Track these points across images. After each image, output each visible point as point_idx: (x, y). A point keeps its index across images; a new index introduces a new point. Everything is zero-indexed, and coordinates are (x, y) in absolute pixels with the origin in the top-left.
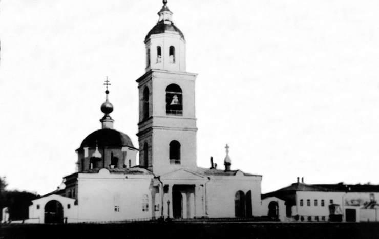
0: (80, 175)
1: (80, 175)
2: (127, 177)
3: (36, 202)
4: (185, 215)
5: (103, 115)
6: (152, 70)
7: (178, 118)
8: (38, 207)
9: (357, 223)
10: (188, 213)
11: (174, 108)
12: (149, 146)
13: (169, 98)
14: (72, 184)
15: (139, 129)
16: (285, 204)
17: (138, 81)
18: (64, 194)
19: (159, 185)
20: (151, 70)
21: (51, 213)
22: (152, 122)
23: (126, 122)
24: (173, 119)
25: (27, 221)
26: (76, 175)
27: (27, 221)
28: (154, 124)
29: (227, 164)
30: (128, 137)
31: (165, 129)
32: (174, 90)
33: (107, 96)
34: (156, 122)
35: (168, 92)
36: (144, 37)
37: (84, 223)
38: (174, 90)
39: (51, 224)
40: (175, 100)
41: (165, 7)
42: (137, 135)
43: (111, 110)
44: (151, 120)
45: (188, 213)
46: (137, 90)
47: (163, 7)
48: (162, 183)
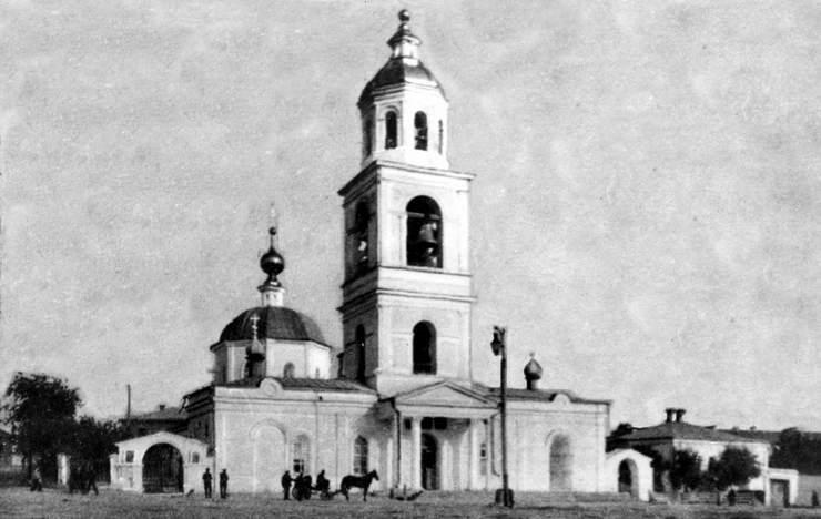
0: (219, 391)
1: (219, 391)
2: (321, 398)
4: (446, 483)
5: (265, 276)
6: (378, 163)
8: (130, 457)
10: (456, 477)
11: (423, 251)
12: (367, 332)
13: (414, 227)
14: (204, 410)
15: (345, 295)
16: (653, 465)
17: (341, 192)
19: (392, 416)
20: (374, 163)
22: (376, 279)
23: (314, 284)
24: (419, 278)
25: (727, 443)
27: (727, 443)
28: (381, 283)
29: (531, 376)
31: (404, 293)
32: (423, 211)
33: (272, 240)
34: (385, 278)
35: (412, 213)
36: (362, 85)
37: (57, 384)
38: (423, 211)
44: (375, 272)
48: (398, 413)
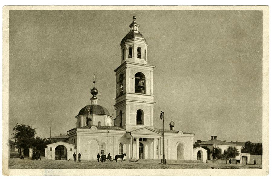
3: (49, 146)
7: (140, 95)
8: (51, 149)
9: (33, 139)
10: (149, 156)
13: (137, 81)
17: (115, 71)
18: (10, 35)
19: (130, 137)
21: (139, 78)
24: (139, 97)
26: (75, 129)
30: (141, 73)
39: (89, 111)
40: (141, 83)
41: (135, 21)
42: (115, 106)
43: (96, 93)
45: (149, 156)
46: (115, 77)
47: (133, 21)
48: (132, 136)
